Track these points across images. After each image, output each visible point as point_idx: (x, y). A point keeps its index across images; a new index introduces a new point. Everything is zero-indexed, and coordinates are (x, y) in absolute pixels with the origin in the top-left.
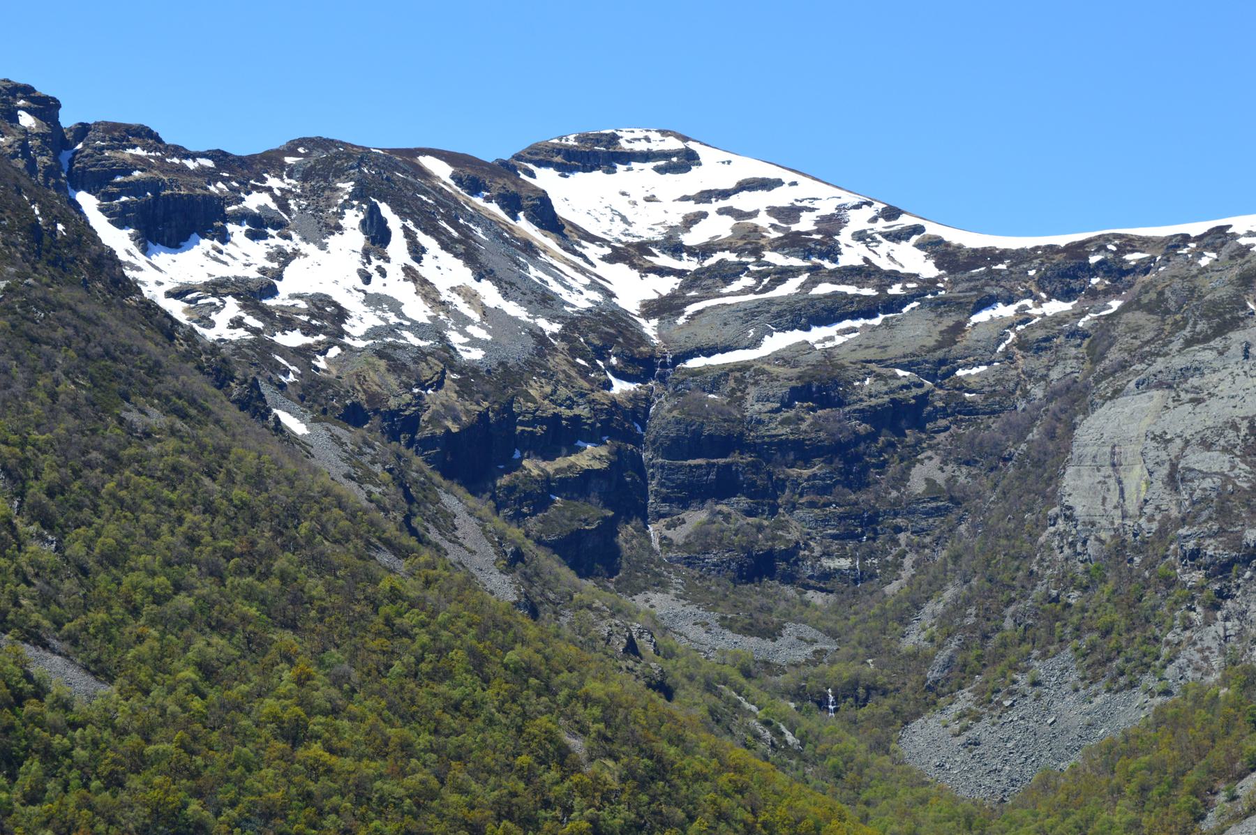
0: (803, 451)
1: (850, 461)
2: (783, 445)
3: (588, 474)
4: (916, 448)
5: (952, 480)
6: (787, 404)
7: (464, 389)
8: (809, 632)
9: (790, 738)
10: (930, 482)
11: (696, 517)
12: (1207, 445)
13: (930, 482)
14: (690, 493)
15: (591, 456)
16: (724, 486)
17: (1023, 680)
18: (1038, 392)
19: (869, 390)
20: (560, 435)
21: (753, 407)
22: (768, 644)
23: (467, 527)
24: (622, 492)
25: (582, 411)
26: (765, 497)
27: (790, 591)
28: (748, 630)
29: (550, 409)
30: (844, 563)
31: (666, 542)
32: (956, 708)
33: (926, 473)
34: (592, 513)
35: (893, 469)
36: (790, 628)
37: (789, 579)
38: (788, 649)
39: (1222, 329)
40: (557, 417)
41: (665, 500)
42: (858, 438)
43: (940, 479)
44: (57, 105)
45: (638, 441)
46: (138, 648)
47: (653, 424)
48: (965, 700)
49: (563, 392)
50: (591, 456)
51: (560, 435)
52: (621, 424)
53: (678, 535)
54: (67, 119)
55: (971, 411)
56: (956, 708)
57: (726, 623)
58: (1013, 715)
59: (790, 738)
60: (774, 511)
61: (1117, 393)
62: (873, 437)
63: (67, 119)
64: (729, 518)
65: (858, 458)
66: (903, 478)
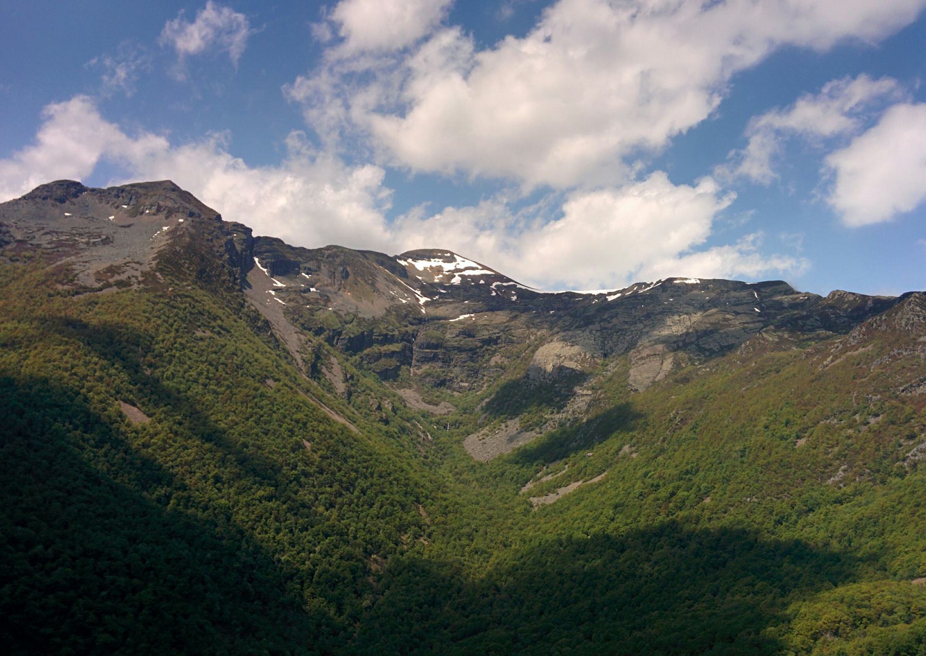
0: (460, 349)
1: (473, 353)
2: (454, 348)
3: (393, 353)
4: (495, 351)
5: (503, 362)
6: (457, 336)
7: (359, 325)
8: (449, 405)
9: (429, 437)
10: (496, 362)
11: (426, 367)
12: (571, 359)
13: (496, 362)
14: (425, 360)
15: (395, 347)
16: (434, 358)
17: (503, 425)
18: (532, 338)
19: (485, 335)
20: (387, 339)
21: (448, 336)
22: (435, 407)
23: (337, 369)
24: (405, 357)
25: (396, 333)
26: (447, 362)
27: (449, 391)
28: (429, 403)
29: (385, 332)
30: (466, 384)
31: (415, 374)
32: (482, 432)
33: (496, 359)
34: (394, 362)
35: (487, 357)
36: (443, 403)
37: (449, 388)
38: (439, 410)
39: (587, 325)
40: (387, 335)
41: (418, 361)
42: (477, 347)
43: (499, 361)
44: (251, 230)
45: (412, 343)
46: (75, 432)
47: (418, 338)
48: (485, 430)
49: (391, 327)
50: (395, 347)
51: (387, 339)
52: (407, 338)
53: (419, 372)
54: (254, 235)
55: (512, 342)
56: (482, 432)
57: (424, 400)
58: (498, 436)
59: (429, 437)
60: (449, 366)
61: (551, 341)
62: (482, 347)
63: (254, 235)
64: (436, 368)
65: (476, 353)
66: (488, 360)
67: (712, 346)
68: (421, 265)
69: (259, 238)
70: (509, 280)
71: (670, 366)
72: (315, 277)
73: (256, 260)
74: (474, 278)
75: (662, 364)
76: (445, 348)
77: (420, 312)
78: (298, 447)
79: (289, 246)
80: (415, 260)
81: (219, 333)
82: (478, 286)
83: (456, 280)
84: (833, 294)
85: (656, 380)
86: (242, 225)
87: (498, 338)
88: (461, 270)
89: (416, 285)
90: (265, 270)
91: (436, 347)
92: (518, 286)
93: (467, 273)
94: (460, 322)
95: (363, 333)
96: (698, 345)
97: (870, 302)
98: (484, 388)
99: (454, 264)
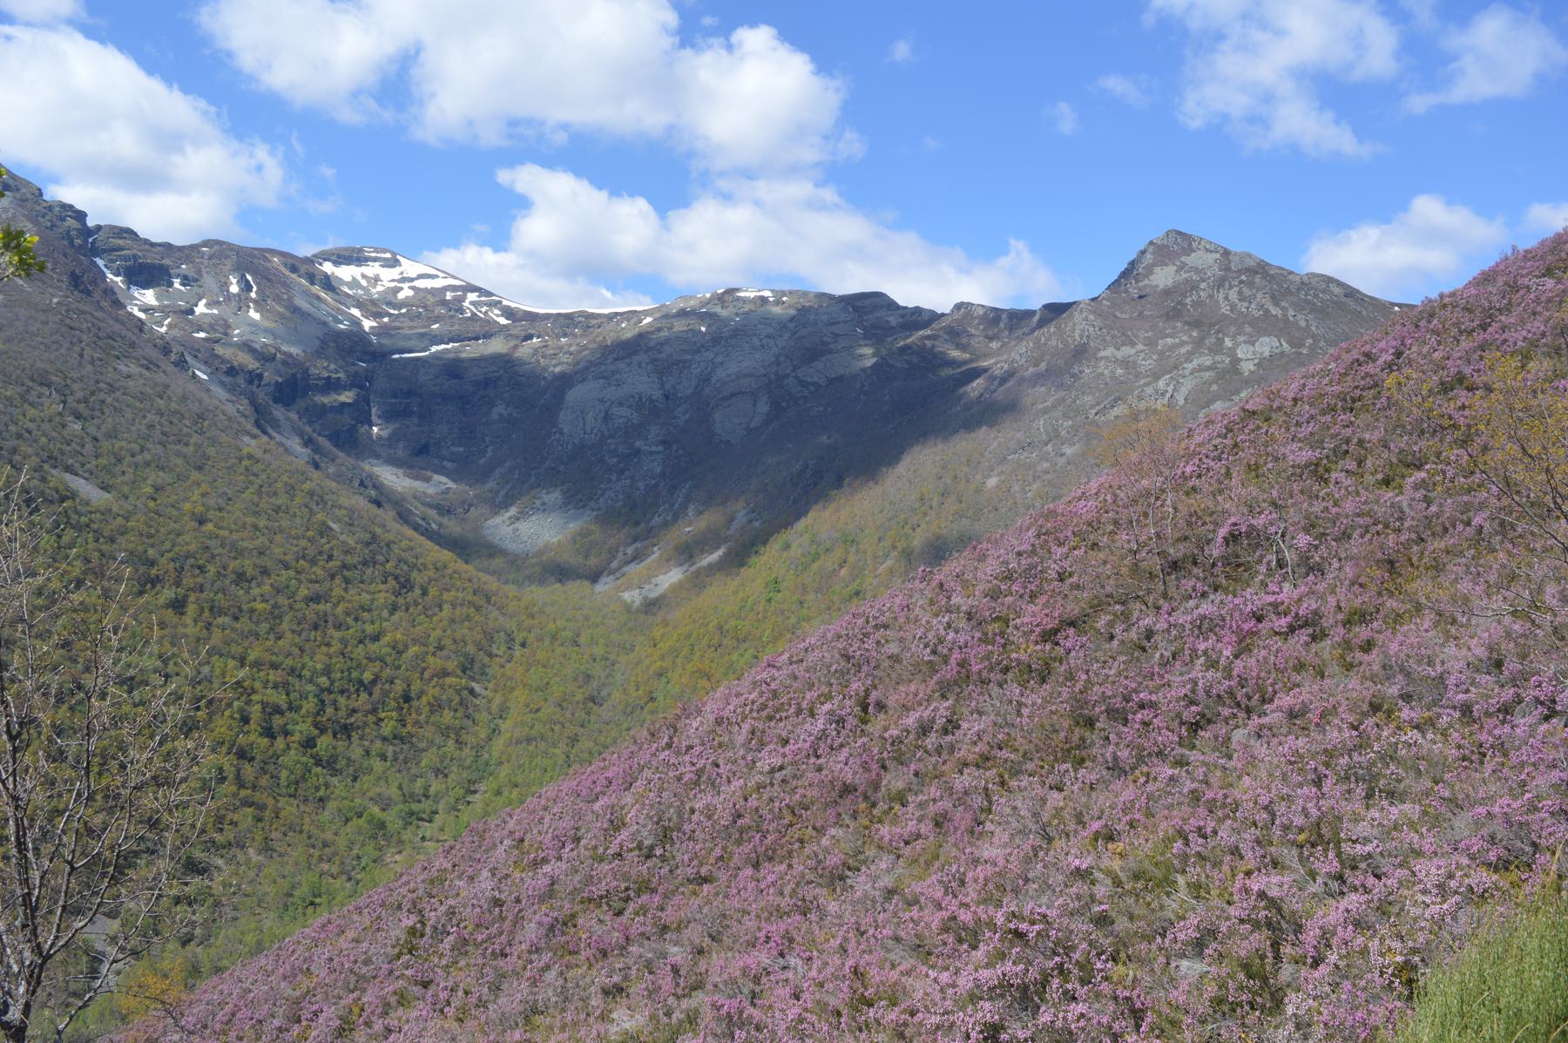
3: (343, 404)
12: (621, 404)
33: (499, 410)
50: (347, 397)
54: (91, 223)
63: (91, 223)
67: (816, 379)
68: (345, 273)
69: (99, 228)
70: (489, 294)
71: (767, 408)
72: (196, 289)
73: (100, 262)
74: (433, 291)
75: (754, 405)
76: (649, 349)
77: (370, 343)
78: (325, 530)
79: (146, 241)
80: (336, 263)
81: (148, 369)
82: (444, 303)
83: (406, 293)
84: (959, 306)
85: (753, 425)
86: (71, 206)
87: (498, 378)
88: (412, 280)
89: (349, 301)
90: (118, 279)
91: (408, 394)
92: (505, 303)
93: (421, 284)
94: (435, 356)
95: (294, 375)
96: (796, 377)
97: (1004, 316)
98: (489, 454)
99: (398, 270)
